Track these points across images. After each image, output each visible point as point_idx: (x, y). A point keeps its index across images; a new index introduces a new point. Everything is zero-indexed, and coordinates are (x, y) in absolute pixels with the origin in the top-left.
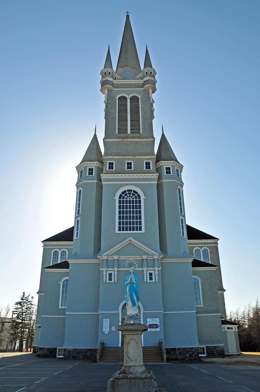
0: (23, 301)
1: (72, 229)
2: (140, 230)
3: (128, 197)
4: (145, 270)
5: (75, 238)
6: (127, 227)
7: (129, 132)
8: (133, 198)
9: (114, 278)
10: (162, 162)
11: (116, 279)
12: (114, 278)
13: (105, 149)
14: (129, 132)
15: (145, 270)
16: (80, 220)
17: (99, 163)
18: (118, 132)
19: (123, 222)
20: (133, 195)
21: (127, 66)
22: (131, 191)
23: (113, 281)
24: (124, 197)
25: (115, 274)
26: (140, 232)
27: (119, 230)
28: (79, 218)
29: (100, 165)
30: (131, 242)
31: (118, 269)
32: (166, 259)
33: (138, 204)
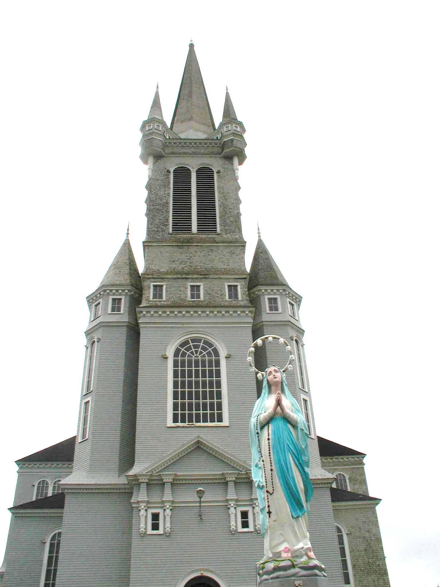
0: (268, 398)
1: (71, 442)
2: (220, 420)
3: (192, 353)
4: (232, 505)
5: (79, 440)
6: (190, 416)
7: (194, 228)
8: (204, 355)
9: (165, 524)
10: (260, 287)
11: (168, 525)
12: (165, 524)
13: (146, 261)
14: (194, 228)
15: (168, 506)
16: (101, 302)
17: (134, 288)
18: (173, 230)
19: (183, 405)
20: (204, 349)
21: (191, 119)
22: (199, 340)
23: (161, 531)
24: (184, 355)
25: (166, 514)
26: (219, 424)
27: (175, 420)
28: (89, 399)
29: (135, 293)
30: (200, 445)
31: (147, 504)
32: (153, 499)
33: (214, 368)
